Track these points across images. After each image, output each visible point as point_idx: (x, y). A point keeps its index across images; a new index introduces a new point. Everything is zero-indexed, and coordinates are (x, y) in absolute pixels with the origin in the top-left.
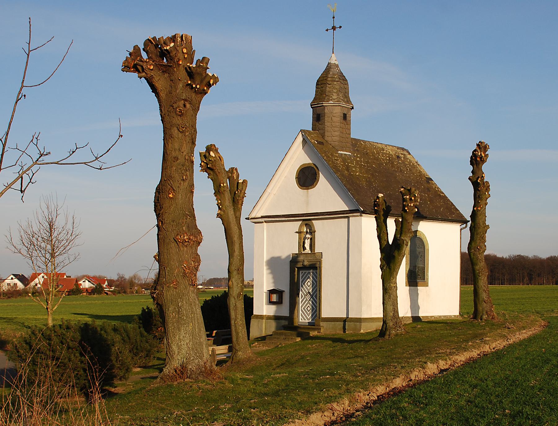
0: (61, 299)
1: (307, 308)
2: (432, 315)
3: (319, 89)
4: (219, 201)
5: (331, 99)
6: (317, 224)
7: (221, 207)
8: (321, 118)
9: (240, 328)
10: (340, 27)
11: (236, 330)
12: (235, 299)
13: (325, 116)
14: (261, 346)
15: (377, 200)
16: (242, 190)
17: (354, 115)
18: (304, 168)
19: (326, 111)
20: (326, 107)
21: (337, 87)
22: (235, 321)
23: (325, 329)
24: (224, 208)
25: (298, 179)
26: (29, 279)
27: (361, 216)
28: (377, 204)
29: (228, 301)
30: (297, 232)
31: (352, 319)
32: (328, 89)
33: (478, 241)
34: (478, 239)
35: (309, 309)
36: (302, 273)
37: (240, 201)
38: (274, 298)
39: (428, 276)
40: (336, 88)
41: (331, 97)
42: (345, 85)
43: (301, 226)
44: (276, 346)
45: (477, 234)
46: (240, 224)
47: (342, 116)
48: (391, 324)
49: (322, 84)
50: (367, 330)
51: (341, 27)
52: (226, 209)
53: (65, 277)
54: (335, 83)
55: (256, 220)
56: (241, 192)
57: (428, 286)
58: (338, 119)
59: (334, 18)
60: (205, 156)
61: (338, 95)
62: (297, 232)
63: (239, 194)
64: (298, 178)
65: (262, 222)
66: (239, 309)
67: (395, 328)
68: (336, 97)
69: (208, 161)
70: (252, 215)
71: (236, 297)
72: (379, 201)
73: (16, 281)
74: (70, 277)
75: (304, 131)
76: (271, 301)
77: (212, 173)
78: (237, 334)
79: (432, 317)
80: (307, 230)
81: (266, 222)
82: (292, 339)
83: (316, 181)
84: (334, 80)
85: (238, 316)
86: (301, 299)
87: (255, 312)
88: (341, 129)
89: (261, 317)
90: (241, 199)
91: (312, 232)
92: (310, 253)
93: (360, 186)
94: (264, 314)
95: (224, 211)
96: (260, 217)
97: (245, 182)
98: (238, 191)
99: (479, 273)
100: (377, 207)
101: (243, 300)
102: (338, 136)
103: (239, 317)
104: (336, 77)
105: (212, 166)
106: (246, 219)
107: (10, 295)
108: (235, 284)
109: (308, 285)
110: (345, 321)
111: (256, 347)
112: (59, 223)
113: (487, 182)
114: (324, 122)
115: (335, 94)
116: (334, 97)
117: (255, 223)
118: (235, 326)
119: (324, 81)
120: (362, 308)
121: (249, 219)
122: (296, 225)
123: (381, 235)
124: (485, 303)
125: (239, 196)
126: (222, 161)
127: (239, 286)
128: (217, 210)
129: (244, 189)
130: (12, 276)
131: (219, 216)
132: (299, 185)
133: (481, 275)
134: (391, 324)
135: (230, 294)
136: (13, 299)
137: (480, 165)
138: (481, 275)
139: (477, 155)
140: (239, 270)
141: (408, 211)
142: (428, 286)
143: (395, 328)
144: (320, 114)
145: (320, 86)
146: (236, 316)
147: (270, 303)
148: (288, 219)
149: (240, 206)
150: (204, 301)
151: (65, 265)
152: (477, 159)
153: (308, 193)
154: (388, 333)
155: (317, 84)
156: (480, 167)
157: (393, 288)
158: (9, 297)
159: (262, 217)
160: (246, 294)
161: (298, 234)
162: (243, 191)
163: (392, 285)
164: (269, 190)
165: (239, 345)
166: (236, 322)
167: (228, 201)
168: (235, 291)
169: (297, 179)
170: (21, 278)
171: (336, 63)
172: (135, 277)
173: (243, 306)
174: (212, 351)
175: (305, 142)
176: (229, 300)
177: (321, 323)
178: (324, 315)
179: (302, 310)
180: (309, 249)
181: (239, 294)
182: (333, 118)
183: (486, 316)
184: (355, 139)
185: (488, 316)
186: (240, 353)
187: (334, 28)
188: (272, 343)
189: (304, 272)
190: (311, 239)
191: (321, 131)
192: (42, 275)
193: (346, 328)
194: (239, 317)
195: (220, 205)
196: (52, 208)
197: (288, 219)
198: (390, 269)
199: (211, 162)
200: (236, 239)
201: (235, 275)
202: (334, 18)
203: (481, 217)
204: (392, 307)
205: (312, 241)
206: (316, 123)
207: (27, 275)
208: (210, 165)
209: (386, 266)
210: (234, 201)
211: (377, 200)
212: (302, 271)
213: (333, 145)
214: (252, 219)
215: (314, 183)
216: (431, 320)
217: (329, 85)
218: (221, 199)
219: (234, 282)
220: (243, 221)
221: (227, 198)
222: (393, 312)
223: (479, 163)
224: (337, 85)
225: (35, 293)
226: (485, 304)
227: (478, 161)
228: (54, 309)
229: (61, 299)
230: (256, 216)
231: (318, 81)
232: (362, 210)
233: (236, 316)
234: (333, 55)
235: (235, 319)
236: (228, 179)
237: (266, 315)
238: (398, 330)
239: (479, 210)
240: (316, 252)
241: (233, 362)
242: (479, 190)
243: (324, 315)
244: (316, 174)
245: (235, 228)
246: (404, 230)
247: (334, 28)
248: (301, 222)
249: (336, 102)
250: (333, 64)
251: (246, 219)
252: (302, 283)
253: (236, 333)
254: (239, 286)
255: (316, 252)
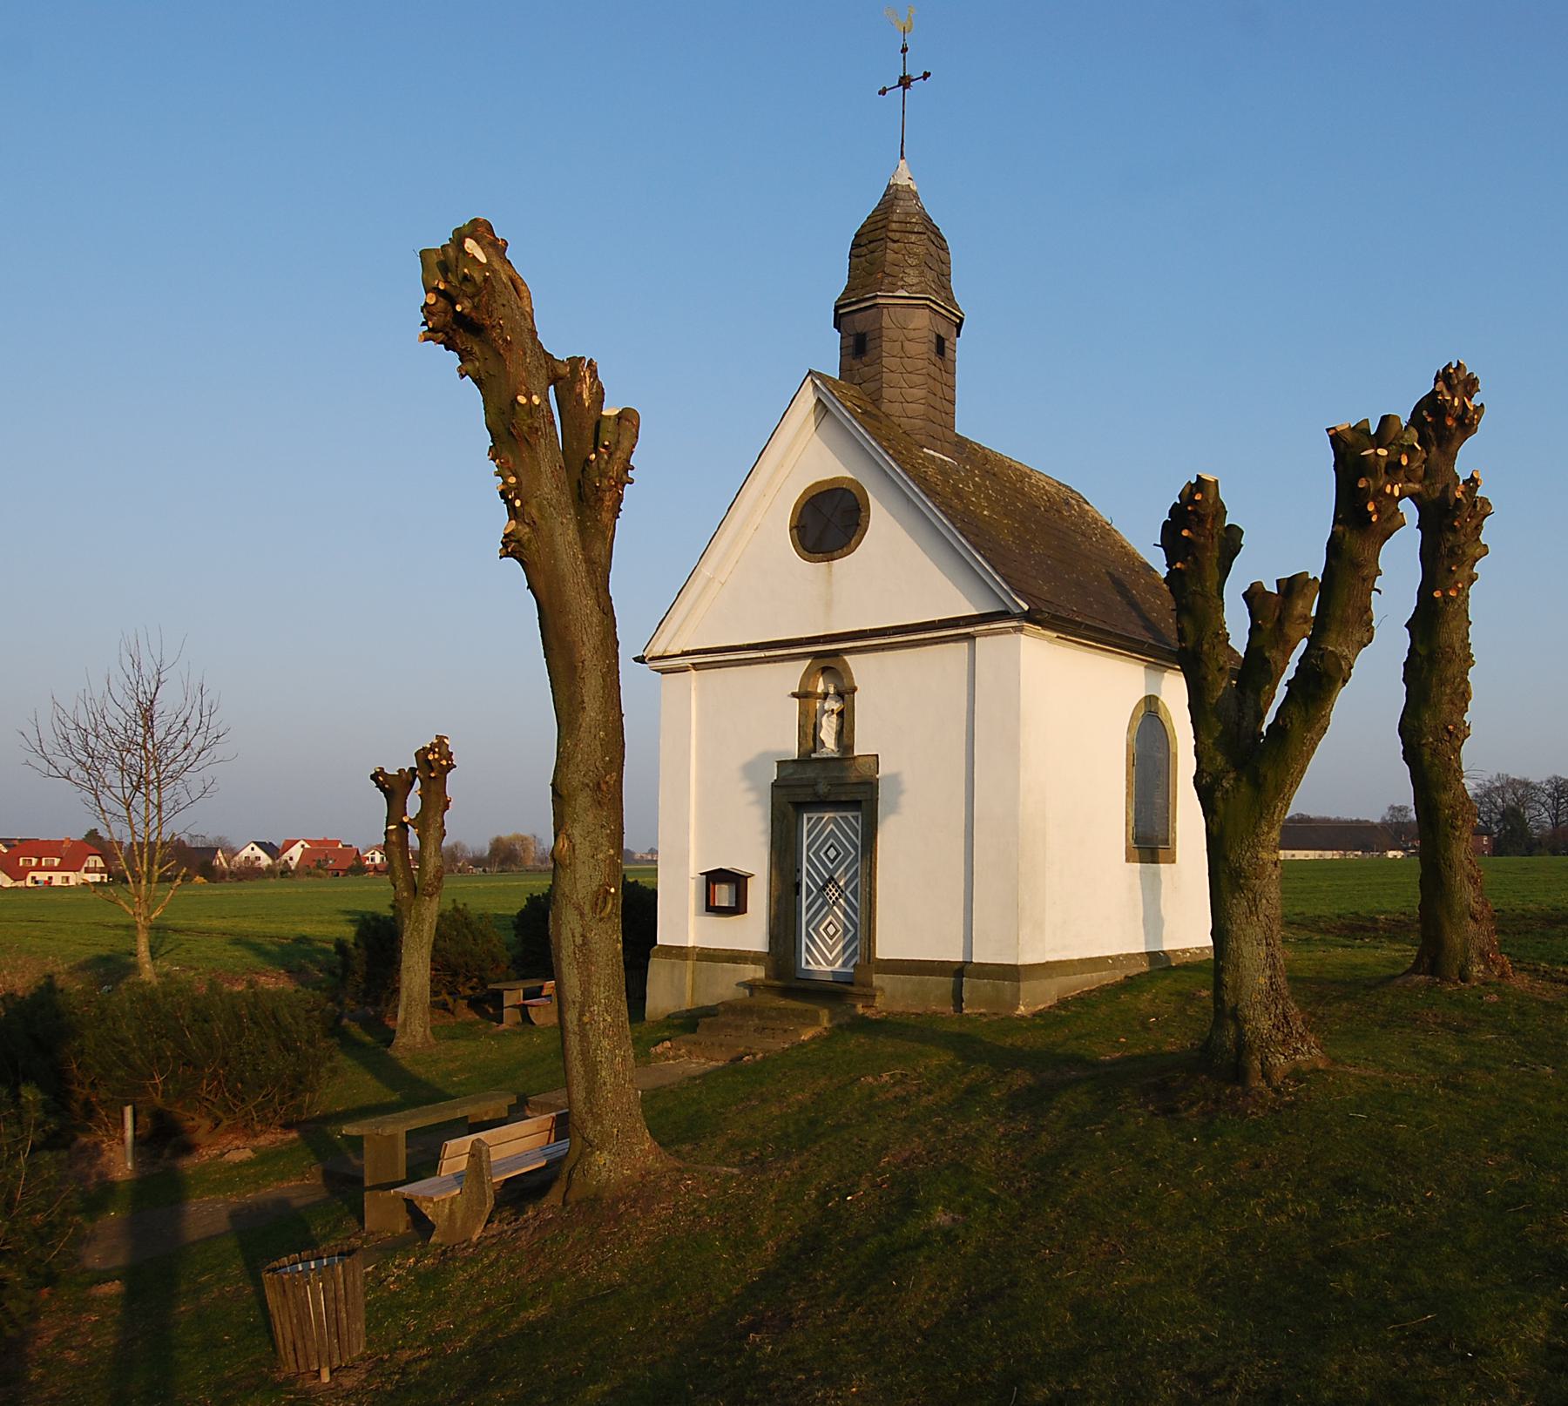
0: (172, 891)
1: (825, 929)
2: (1183, 947)
3: (863, 259)
4: (512, 480)
5: (900, 283)
6: (860, 667)
7: (518, 503)
8: (870, 345)
9: (605, 1043)
10: (926, 75)
11: (584, 1053)
12: (582, 915)
13: (881, 337)
14: (681, 1052)
15: (1198, 497)
16: (617, 449)
17: (964, 348)
18: (817, 494)
19: (886, 321)
20: (885, 311)
21: (920, 250)
22: (581, 1014)
23: (890, 995)
24: (534, 512)
25: (799, 531)
26: (280, 848)
27: (1019, 630)
28: (1194, 512)
29: (551, 923)
30: (794, 695)
31: (986, 968)
32: (890, 256)
33: (1446, 707)
34: (1446, 698)
35: (831, 930)
36: (809, 820)
37: (608, 496)
38: (724, 895)
39: (1175, 833)
40: (915, 254)
41: (902, 279)
42: (941, 251)
43: (807, 674)
44: (734, 1054)
45: (1442, 683)
46: (619, 683)
47: (934, 341)
48: (1265, 1025)
49: (870, 242)
50: (1036, 1005)
51: (929, 74)
52: (543, 517)
53: (340, 846)
54: (913, 238)
55: (665, 664)
56: (610, 455)
57: (1174, 862)
58: (921, 349)
59: (904, 50)
60: (445, 268)
61: (922, 274)
62: (794, 695)
63: (603, 466)
64: (796, 527)
65: (685, 670)
66: (602, 960)
67: (1284, 1043)
68: (915, 281)
69: (455, 283)
70: (654, 649)
71: (587, 909)
72: (1205, 499)
73: (259, 852)
74: (351, 846)
75: (820, 376)
76: (711, 904)
77: (476, 349)
78: (592, 1069)
79: (1184, 951)
80: (826, 687)
81: (695, 666)
82: (785, 1031)
83: (859, 532)
84: (908, 229)
85: (594, 989)
86: (807, 899)
87: (662, 939)
88: (931, 381)
89: (680, 953)
90: (610, 488)
91: (846, 693)
92: (837, 758)
93: (1000, 545)
94: (690, 944)
95: (533, 525)
96: (679, 653)
97: (628, 418)
98: (596, 451)
99: (1454, 816)
100: (1190, 529)
101: (618, 920)
102: (923, 401)
103: (601, 994)
104: (914, 220)
105: (475, 308)
106: (636, 659)
107: (242, 877)
108: (583, 849)
109: (828, 857)
110: (959, 971)
111: (668, 1059)
112: (168, 705)
113: (1485, 501)
114: (880, 357)
115: (911, 272)
116: (909, 280)
117: (664, 672)
118: (584, 1037)
119: (879, 231)
120: (1020, 933)
121: (643, 662)
122: (792, 674)
123: (1206, 647)
124: (1472, 923)
125: (603, 474)
126: (526, 302)
127: (600, 856)
128: (499, 520)
129: (625, 444)
130: (253, 845)
131: (512, 547)
132: (801, 550)
133: (1460, 823)
134: (1265, 1025)
135: (559, 892)
136: (247, 883)
137: (1456, 444)
138: (1460, 823)
139: (1448, 405)
140: (604, 787)
141: (1374, 519)
142: (1174, 862)
143: (1284, 1043)
144: (864, 334)
145: (864, 250)
146: (586, 992)
147: (707, 911)
148: (768, 654)
149: (606, 516)
150: (527, 899)
151: (181, 807)
152: (1444, 422)
153: (831, 571)
154: (1257, 1064)
155: (855, 245)
156: (1452, 449)
157: (1270, 867)
158: (240, 880)
159: (685, 654)
160: (636, 881)
161: (797, 700)
162: (618, 454)
163: (1264, 855)
164: (706, 571)
165: (598, 1119)
166: (586, 1019)
167: (550, 487)
168: (586, 879)
169: (795, 531)
170: (267, 847)
171: (911, 187)
172: (456, 846)
173: (620, 946)
174: (472, 1155)
175: (821, 406)
176: (557, 919)
177: (874, 976)
178: (884, 951)
179: (809, 936)
180: (833, 747)
181: (601, 896)
182: (906, 344)
183: (1482, 967)
184: (407, 1173)
185: (1487, 966)
186: (602, 1158)
187: (905, 82)
188: (721, 1045)
189: (815, 816)
190: (841, 714)
191: (871, 386)
192: (302, 842)
193: (965, 996)
194: (601, 994)
195: (516, 497)
196: (148, 670)
197: (768, 654)
198: (1257, 784)
199: (469, 289)
200: (587, 651)
201: (586, 810)
202: (904, 50)
203: (1455, 623)
204: (1263, 951)
205: (845, 719)
206: (854, 362)
207: (278, 843)
208: (468, 303)
209: (1232, 775)
210: (580, 495)
211: (1198, 497)
212: (810, 815)
213: (908, 428)
214: (653, 659)
215: (851, 540)
216: (1185, 960)
217: (896, 245)
218: (521, 471)
219: (578, 840)
220: (628, 671)
221: (546, 467)
222: (1268, 972)
223: (1452, 435)
224: (919, 245)
225: (286, 872)
226: (1472, 926)
227: (1449, 428)
228: (153, 916)
229: (172, 891)
230: (665, 651)
231: (857, 236)
232: (1026, 607)
233: (586, 992)
234: (902, 162)
235: (583, 1005)
236: (552, 387)
237: (694, 947)
238: (1296, 1050)
239: (1453, 600)
240: (856, 754)
241: (571, 1197)
242: (1454, 530)
243: (884, 951)
244: (859, 509)
245: (582, 605)
246: (1339, 613)
247: (905, 82)
248: (810, 661)
249: (917, 293)
250: (902, 186)
251: (636, 659)
252: (808, 851)
253: (584, 1065)
254: (600, 856)
255: (856, 754)
